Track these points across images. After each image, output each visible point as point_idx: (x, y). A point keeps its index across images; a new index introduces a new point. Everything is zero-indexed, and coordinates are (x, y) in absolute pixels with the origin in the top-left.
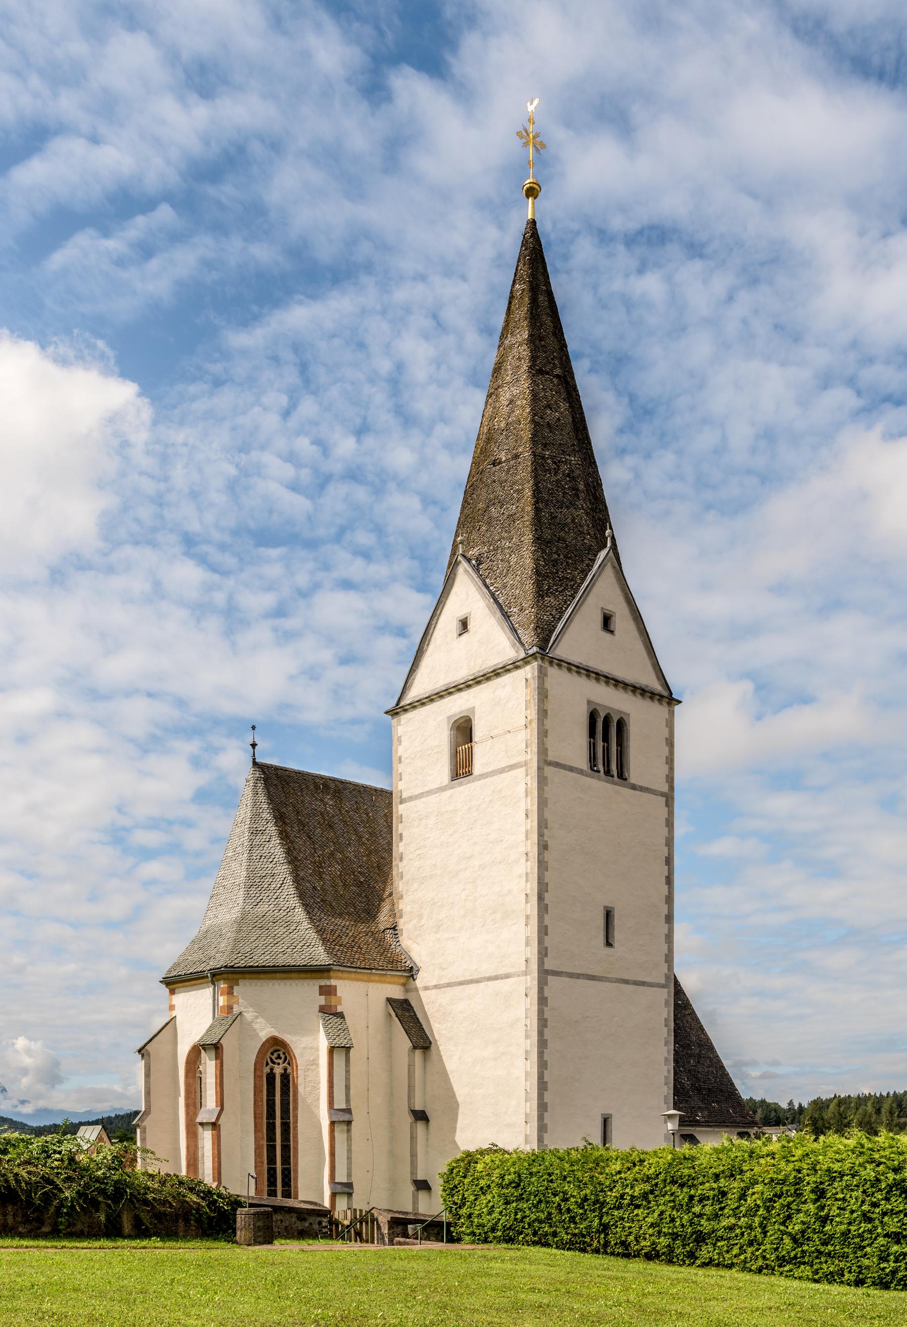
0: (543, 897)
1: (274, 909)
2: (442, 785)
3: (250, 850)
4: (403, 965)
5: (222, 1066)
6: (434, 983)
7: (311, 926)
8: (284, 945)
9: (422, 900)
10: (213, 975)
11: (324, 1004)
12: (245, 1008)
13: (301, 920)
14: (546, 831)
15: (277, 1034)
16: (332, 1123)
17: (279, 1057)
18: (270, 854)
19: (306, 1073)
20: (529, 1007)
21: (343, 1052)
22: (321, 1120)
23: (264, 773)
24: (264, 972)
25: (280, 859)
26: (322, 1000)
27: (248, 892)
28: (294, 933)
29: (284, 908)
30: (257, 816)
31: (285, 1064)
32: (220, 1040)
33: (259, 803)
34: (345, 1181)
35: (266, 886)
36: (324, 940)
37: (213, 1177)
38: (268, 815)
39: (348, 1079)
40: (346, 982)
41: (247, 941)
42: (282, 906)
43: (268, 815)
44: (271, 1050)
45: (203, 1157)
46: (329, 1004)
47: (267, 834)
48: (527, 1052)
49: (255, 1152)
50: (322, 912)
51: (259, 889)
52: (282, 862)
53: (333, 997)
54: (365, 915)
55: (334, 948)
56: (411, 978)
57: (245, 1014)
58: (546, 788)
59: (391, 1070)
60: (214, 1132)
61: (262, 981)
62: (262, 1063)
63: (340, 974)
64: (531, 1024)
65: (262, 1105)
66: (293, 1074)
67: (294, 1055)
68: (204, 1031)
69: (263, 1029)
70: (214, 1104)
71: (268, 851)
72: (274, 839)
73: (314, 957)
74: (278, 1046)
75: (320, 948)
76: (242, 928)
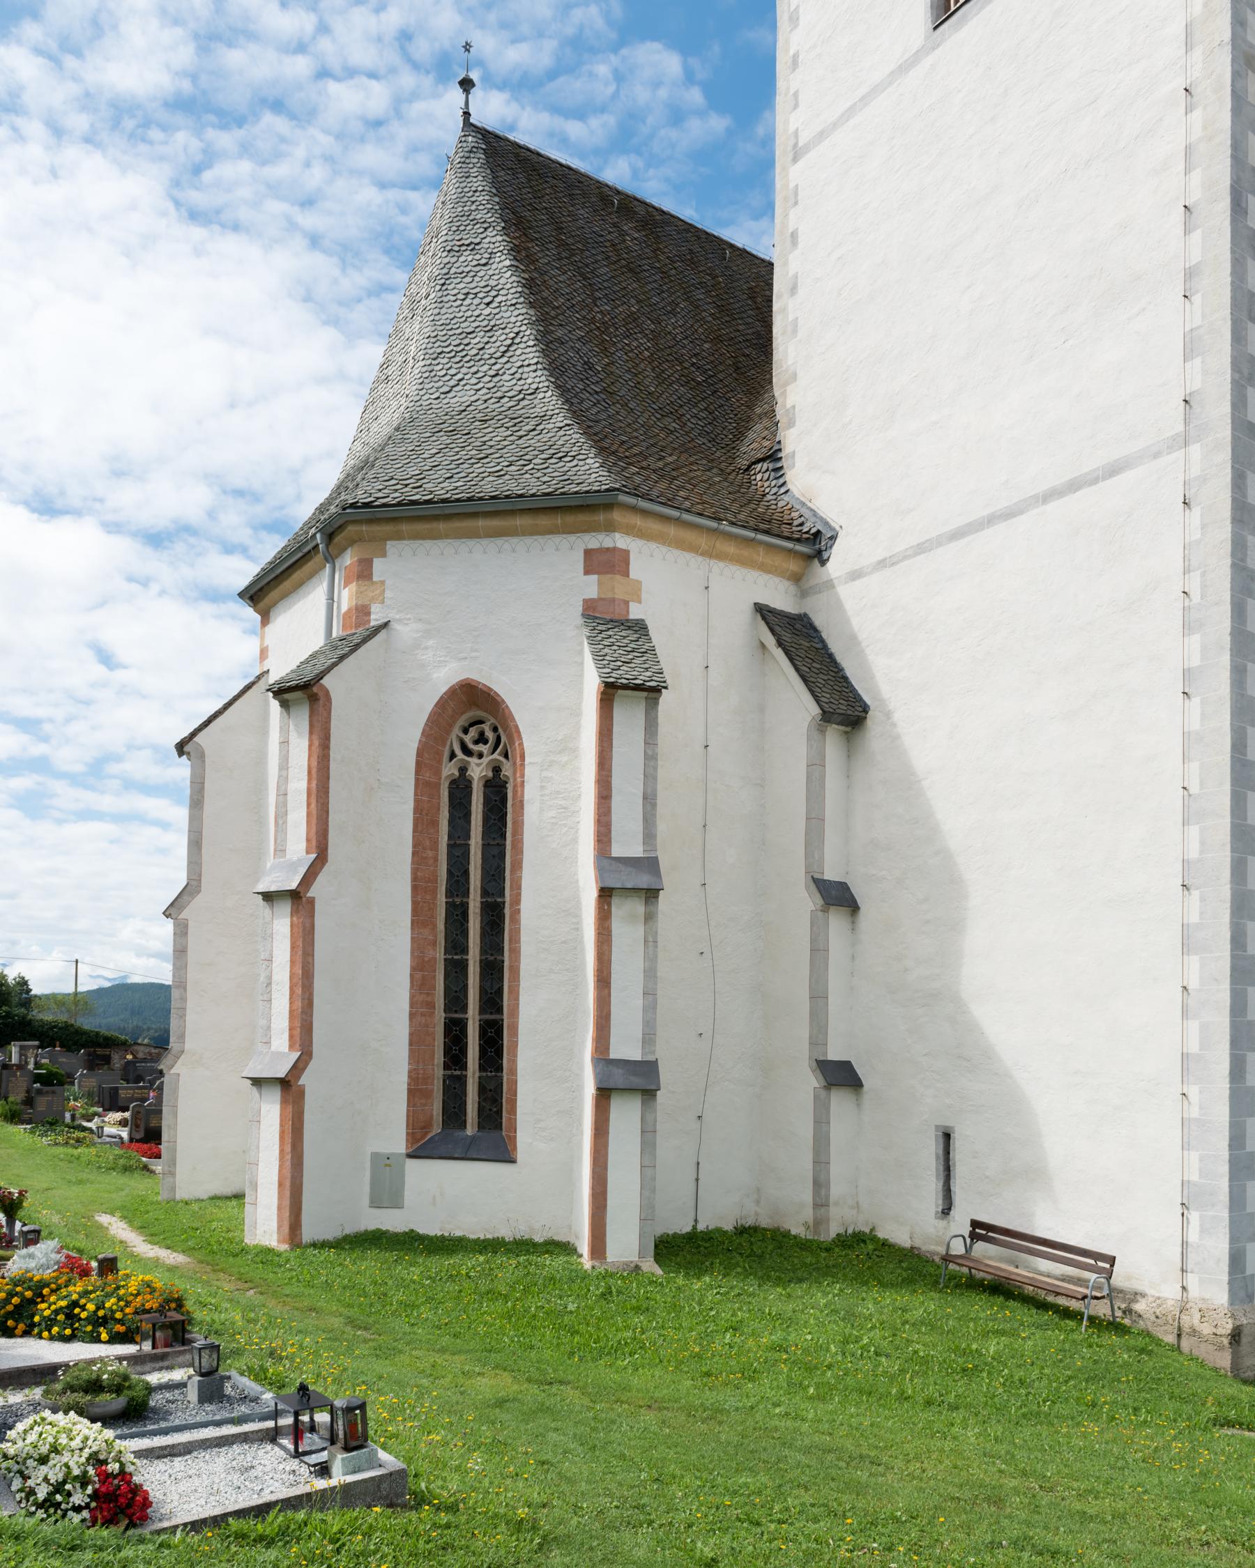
0: (1244, 205)
1: (489, 396)
3: (443, 285)
4: (794, 529)
6: (880, 554)
13: (550, 413)
16: (606, 894)
17: (481, 739)
18: (489, 288)
19: (545, 774)
20: (1197, 535)
23: (487, 143)
24: (448, 517)
25: (510, 297)
26: (590, 587)
28: (529, 437)
30: (465, 218)
31: (496, 756)
34: (637, 1056)
35: (474, 352)
37: (291, 1037)
38: (490, 215)
39: (650, 777)
40: (653, 545)
44: (462, 721)
46: (609, 595)
47: (483, 251)
48: (1187, 674)
51: (457, 359)
52: (514, 301)
53: (618, 577)
54: (706, 441)
56: (816, 561)
61: (441, 544)
62: (440, 754)
63: (637, 521)
64: (1204, 586)
65: (436, 859)
66: (515, 780)
70: (303, 845)
71: (482, 284)
72: (497, 260)
74: (478, 707)
76: (406, 437)
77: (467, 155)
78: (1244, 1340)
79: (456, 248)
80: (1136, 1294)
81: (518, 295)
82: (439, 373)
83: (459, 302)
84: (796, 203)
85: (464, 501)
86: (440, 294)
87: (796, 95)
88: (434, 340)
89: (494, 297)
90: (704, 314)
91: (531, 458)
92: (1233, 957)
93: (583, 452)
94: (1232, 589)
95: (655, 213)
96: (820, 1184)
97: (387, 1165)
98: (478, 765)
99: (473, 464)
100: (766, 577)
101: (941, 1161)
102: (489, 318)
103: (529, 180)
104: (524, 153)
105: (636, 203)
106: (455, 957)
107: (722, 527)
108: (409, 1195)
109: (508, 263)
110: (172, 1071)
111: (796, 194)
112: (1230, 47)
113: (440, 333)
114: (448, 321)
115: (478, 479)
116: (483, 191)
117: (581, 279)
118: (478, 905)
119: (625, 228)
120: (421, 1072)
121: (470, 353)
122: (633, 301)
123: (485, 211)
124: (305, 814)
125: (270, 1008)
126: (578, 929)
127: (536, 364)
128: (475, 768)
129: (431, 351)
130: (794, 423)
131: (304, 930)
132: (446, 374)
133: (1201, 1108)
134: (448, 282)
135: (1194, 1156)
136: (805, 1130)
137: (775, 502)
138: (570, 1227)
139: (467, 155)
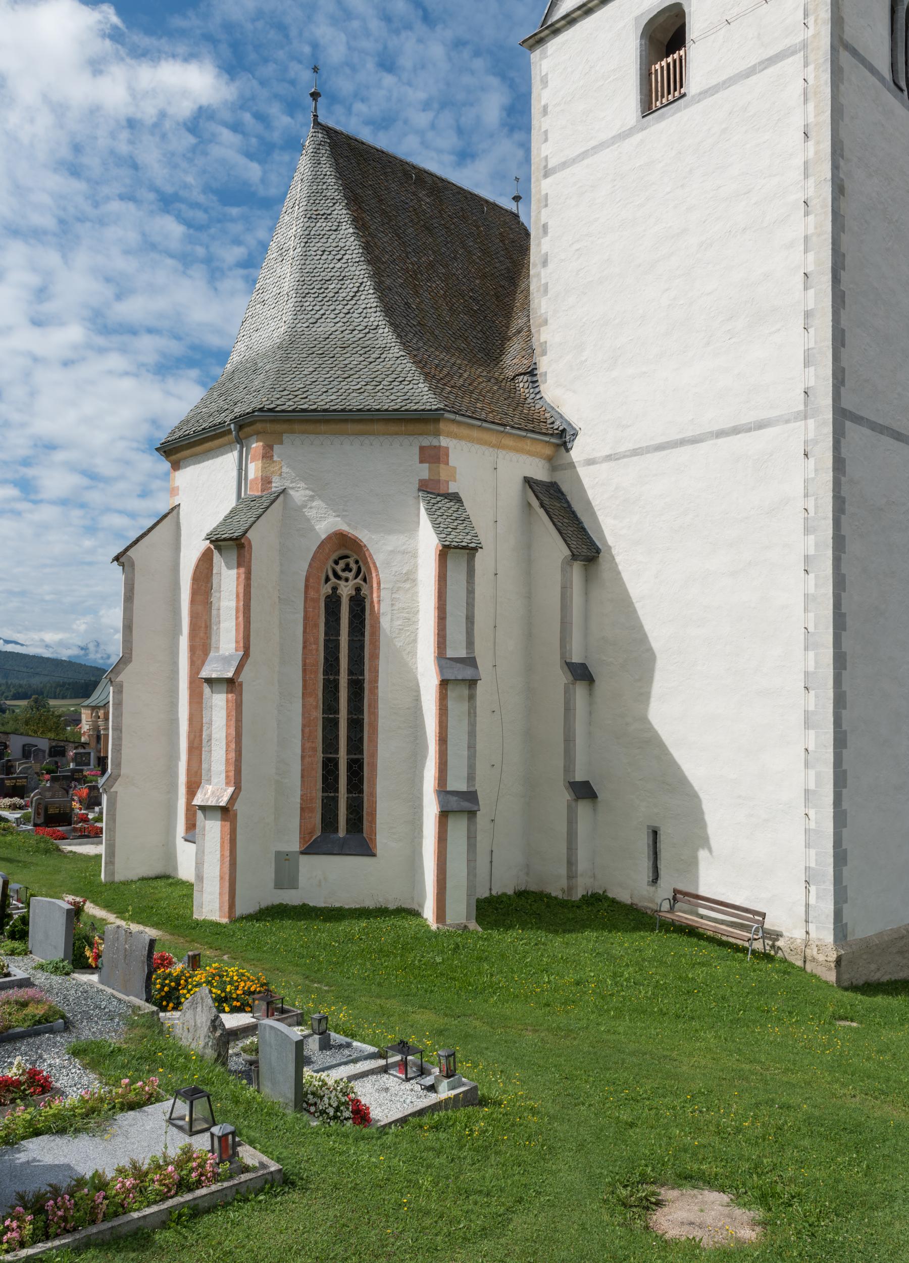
1: (344, 328)
2: (624, 129)
3: (306, 243)
4: (548, 426)
5: (248, 578)
6: (607, 451)
7: (405, 354)
8: (360, 380)
9: (584, 320)
10: (240, 427)
11: (427, 478)
12: (292, 482)
13: (388, 345)
14: (842, 163)
15: (345, 528)
16: (444, 684)
17: (347, 568)
18: (339, 248)
19: (394, 596)
20: (812, 475)
21: (464, 555)
22: (419, 677)
23: (330, 137)
24: (327, 421)
25: (354, 256)
26: (424, 471)
27: (301, 304)
28: (376, 363)
29: (359, 328)
30: (319, 195)
31: (358, 580)
32: (246, 532)
33: (322, 177)
35: (331, 294)
36: (426, 375)
37: (227, 777)
38: (336, 194)
40: (463, 443)
41: (298, 373)
42: (356, 324)
43: (336, 194)
44: (335, 556)
45: (210, 740)
47: (333, 220)
48: (807, 558)
49: (303, 731)
50: (420, 340)
51: (320, 299)
52: (357, 260)
54: (483, 356)
55: (443, 389)
56: (563, 448)
57: (291, 492)
58: (842, 87)
59: (529, 596)
60: (230, 696)
64: (816, 507)
65: (317, 650)
66: (372, 598)
67: (374, 564)
68: (220, 517)
69: (322, 519)
70: (233, 645)
71: (334, 244)
72: (344, 228)
73: (411, 398)
75: (421, 385)
76: (289, 355)
77: (317, 147)
78: (843, 963)
79: (314, 217)
80: (778, 935)
81: (360, 255)
82: (307, 308)
83: (318, 257)
84: (546, 206)
85: (339, 411)
86: (304, 249)
87: (546, 132)
88: (303, 283)
89: (343, 255)
90: (474, 257)
91: (381, 380)
92: (835, 732)
93: (415, 378)
94: (833, 511)
95: (438, 182)
96: (571, 863)
97: (286, 860)
98: (346, 586)
99: (341, 382)
100: (531, 458)
101: (651, 848)
102: (341, 270)
103: (359, 164)
104: (353, 143)
105: (426, 174)
106: (330, 716)
107: (507, 430)
108: (302, 880)
109: (351, 230)
110: (112, 790)
111: (546, 200)
112: (830, 183)
113: (306, 279)
114: (312, 270)
115: (346, 394)
116: (331, 175)
117: (397, 238)
118: (346, 681)
119: (421, 195)
120: (309, 795)
121: (328, 295)
122: (430, 252)
123: (333, 191)
124: (234, 624)
125: (211, 756)
126: (417, 700)
127: (376, 307)
128: (344, 588)
129: (299, 291)
130: (546, 352)
131: (236, 705)
132: (313, 309)
133: (816, 823)
134: (309, 241)
135: (813, 852)
136: (562, 828)
137: (533, 405)
138: (413, 898)
139: (317, 147)
